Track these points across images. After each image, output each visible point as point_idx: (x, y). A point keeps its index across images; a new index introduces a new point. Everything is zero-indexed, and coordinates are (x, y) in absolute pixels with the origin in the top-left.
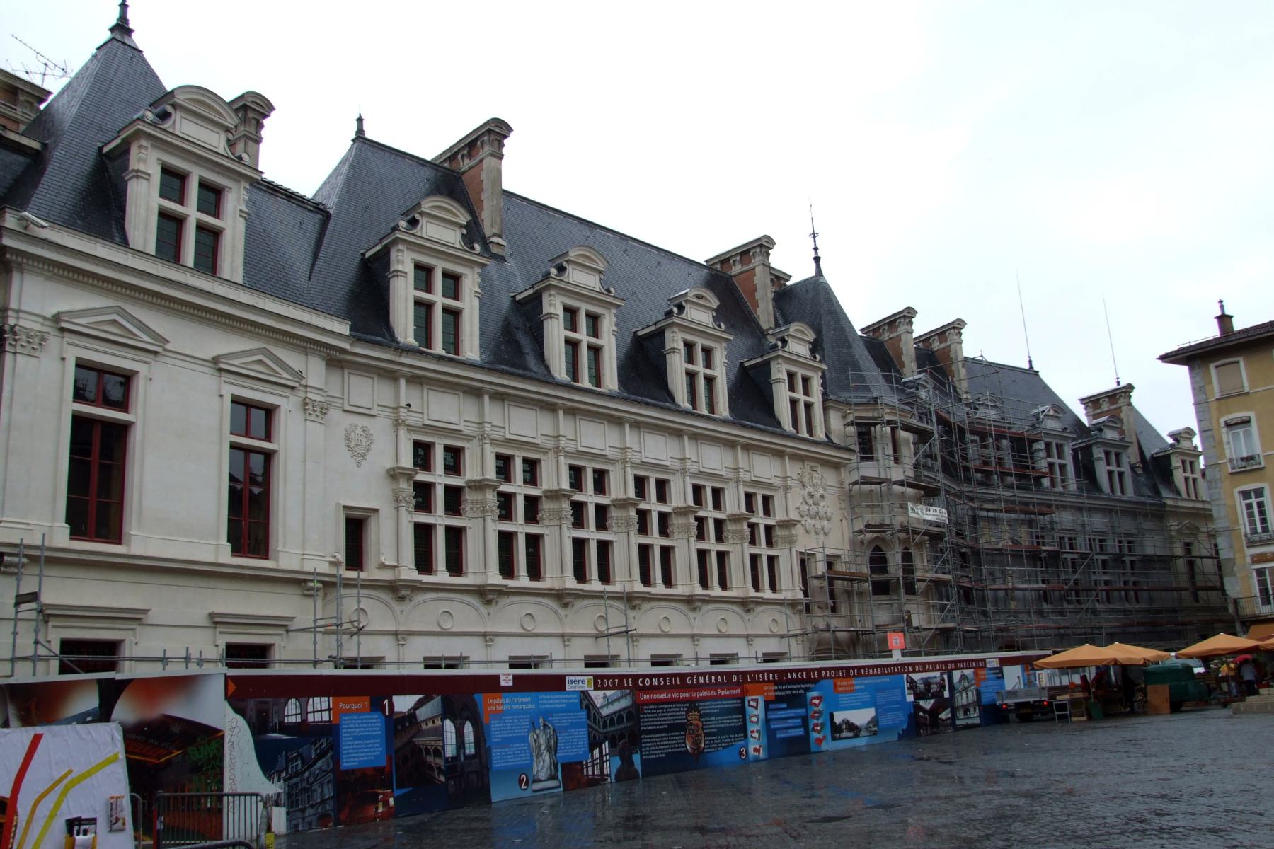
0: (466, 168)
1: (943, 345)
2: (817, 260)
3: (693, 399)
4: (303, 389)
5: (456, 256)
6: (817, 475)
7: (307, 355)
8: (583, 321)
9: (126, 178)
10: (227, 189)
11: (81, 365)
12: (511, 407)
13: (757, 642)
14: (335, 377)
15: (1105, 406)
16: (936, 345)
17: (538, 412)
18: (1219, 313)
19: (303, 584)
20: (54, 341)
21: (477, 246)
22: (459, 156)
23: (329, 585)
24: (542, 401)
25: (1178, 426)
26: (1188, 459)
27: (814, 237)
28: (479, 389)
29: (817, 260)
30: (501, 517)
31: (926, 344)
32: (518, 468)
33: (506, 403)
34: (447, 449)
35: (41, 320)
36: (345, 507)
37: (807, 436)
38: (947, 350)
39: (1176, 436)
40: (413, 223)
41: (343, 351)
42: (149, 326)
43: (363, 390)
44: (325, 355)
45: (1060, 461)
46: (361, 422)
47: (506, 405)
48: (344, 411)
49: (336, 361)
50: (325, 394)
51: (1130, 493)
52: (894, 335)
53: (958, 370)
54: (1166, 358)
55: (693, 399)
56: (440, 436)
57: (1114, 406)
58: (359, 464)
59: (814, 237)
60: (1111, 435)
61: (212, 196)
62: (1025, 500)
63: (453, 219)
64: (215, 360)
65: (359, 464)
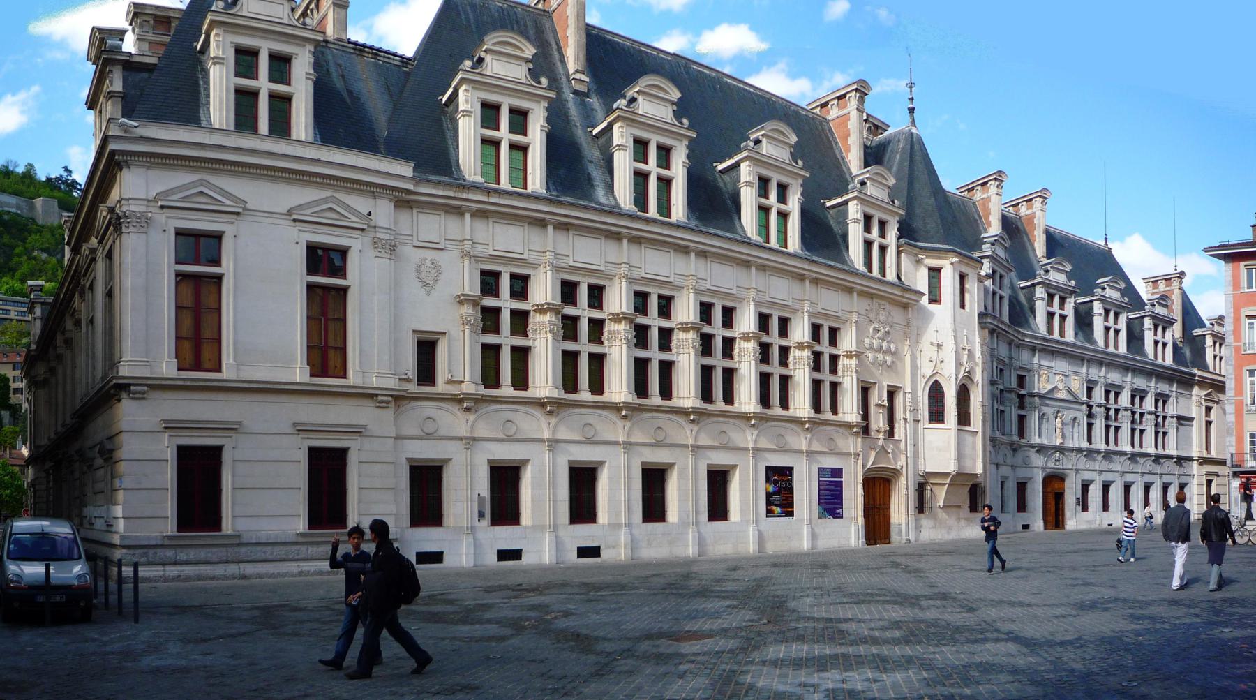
1: (1029, 212)
2: (912, 110)
3: (868, 264)
4: (373, 230)
5: (522, 91)
6: (884, 313)
10: (294, 56)
11: (180, 233)
15: (1162, 286)
16: (1024, 210)
17: (603, 241)
20: (161, 217)
21: (544, 81)
23: (399, 399)
28: (544, 220)
31: (1016, 208)
32: (583, 294)
33: (571, 233)
34: (514, 277)
35: (145, 203)
36: (414, 331)
37: (879, 276)
38: (1031, 218)
41: (408, 192)
42: (230, 191)
43: (430, 226)
44: (391, 197)
45: (1115, 326)
46: (430, 255)
48: (414, 246)
49: (404, 201)
50: (394, 233)
52: (985, 196)
53: (1039, 236)
54: (1206, 250)
55: (868, 264)
57: (1168, 288)
58: (429, 293)
59: (911, 87)
60: (1159, 310)
63: (517, 54)
64: (290, 213)
65: (429, 293)
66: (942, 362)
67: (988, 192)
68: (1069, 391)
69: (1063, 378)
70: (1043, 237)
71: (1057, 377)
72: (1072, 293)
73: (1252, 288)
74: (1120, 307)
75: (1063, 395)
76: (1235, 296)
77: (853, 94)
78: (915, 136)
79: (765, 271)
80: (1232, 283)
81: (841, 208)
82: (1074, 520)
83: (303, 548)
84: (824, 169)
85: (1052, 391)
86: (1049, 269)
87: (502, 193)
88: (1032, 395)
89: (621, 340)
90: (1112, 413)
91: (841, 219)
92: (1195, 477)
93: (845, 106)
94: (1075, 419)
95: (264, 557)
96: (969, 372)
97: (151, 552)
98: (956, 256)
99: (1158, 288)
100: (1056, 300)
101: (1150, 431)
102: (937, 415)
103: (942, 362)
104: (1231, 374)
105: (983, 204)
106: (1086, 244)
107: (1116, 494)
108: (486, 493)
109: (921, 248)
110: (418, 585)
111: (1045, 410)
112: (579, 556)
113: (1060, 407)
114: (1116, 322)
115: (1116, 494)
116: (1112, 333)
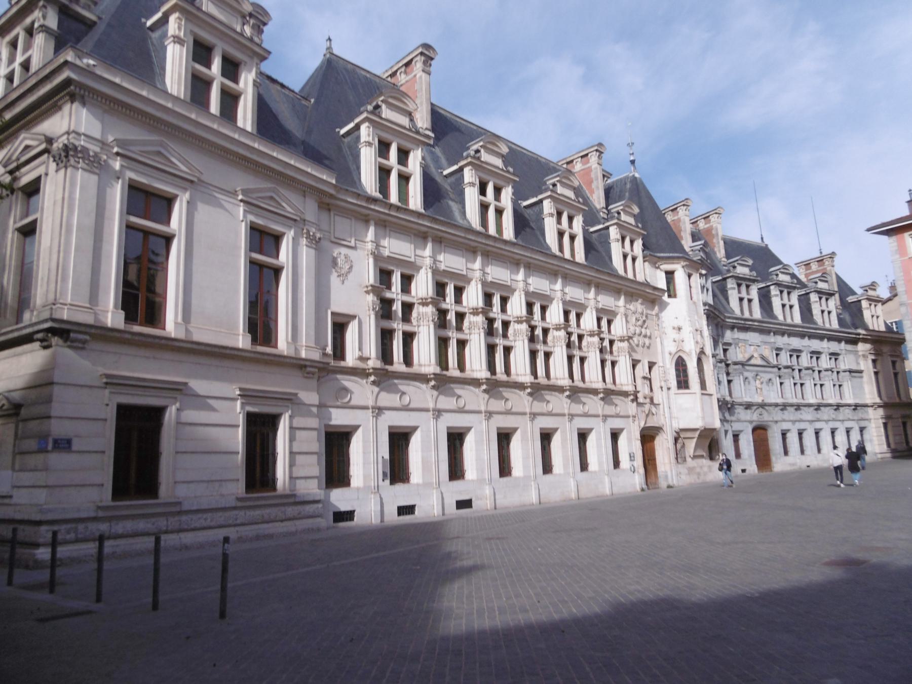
0: (403, 81)
1: (707, 226)
7: (305, 197)
9: (166, 43)
10: (243, 63)
12: (446, 248)
13: (797, 423)
14: (324, 215)
15: (814, 267)
16: (702, 225)
19: (304, 369)
22: (398, 73)
24: (466, 244)
25: (868, 282)
26: (873, 304)
31: (695, 225)
39: (866, 289)
51: (835, 325)
52: (676, 218)
54: (869, 230)
60: (821, 285)
61: (231, 69)
66: (683, 341)
67: (678, 215)
68: (763, 358)
69: (757, 347)
70: (722, 243)
71: (752, 347)
72: (754, 281)
74: (749, 280)
75: (757, 361)
77: (418, 58)
78: (638, 179)
79: (385, 226)
81: (602, 232)
82: (780, 464)
83: (242, 513)
85: (750, 359)
86: (736, 265)
89: (479, 329)
90: (574, 338)
91: (603, 240)
92: (872, 421)
93: (412, 71)
94: (770, 380)
95: (205, 524)
96: (702, 348)
97: (81, 527)
98: (685, 261)
100: (743, 288)
101: (593, 360)
102: (683, 383)
105: (674, 224)
106: (748, 244)
107: (809, 439)
108: (387, 456)
109: (659, 258)
111: (746, 374)
112: (399, 514)
113: (757, 371)
114: (570, 227)
115: (809, 439)
116: (745, 302)
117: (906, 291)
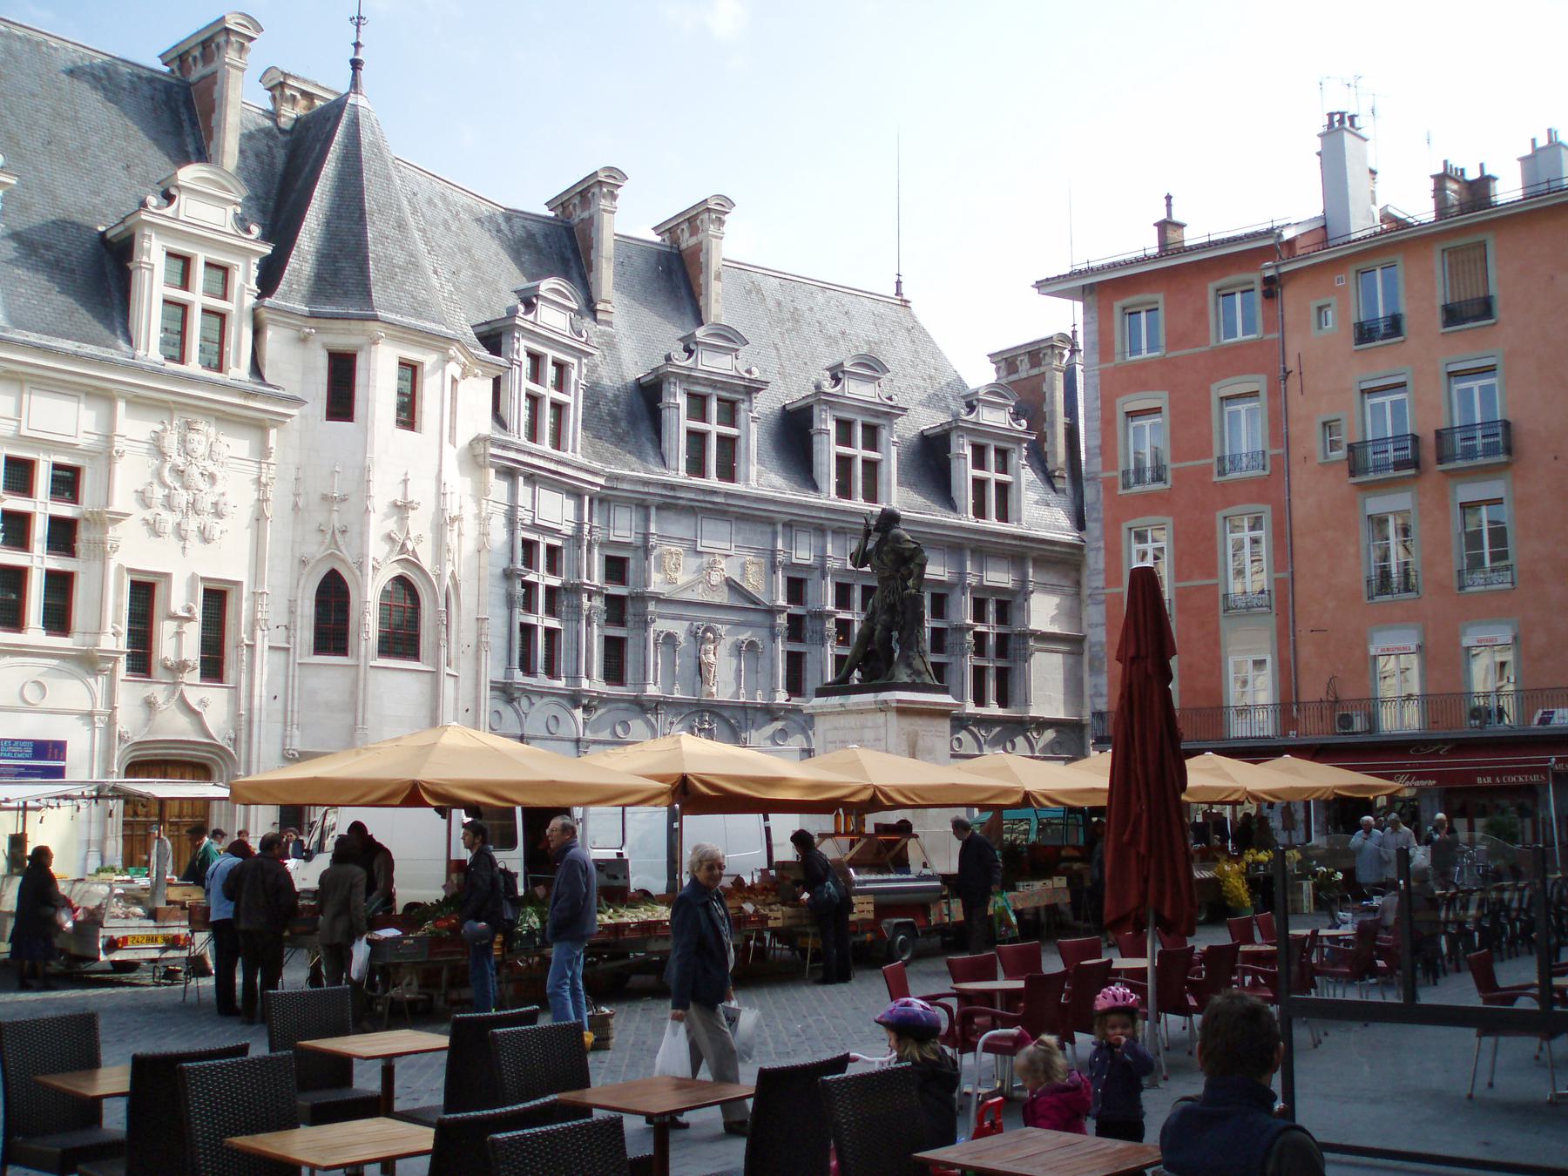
1: (1035, 371)
2: (356, 65)
8: (199, 273)
18: (1163, 216)
27: (358, 25)
29: (356, 65)
30: (609, 621)
38: (697, 250)
40: (169, 198)
47: (699, 518)
54: (1043, 285)
56: (47, 452)
59: (358, 25)
62: (742, 510)
66: (344, 532)
73: (1139, 351)
76: (1103, 373)
80: (1097, 347)
84: (136, 171)
87: (140, 370)
88: (642, 598)
99: (1016, 371)
103: (344, 532)
104: (1097, 540)
110: (392, 860)
113: (711, 620)
117: (1101, 447)
